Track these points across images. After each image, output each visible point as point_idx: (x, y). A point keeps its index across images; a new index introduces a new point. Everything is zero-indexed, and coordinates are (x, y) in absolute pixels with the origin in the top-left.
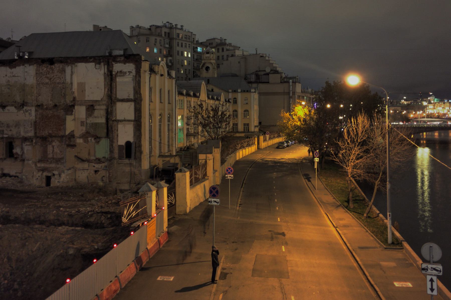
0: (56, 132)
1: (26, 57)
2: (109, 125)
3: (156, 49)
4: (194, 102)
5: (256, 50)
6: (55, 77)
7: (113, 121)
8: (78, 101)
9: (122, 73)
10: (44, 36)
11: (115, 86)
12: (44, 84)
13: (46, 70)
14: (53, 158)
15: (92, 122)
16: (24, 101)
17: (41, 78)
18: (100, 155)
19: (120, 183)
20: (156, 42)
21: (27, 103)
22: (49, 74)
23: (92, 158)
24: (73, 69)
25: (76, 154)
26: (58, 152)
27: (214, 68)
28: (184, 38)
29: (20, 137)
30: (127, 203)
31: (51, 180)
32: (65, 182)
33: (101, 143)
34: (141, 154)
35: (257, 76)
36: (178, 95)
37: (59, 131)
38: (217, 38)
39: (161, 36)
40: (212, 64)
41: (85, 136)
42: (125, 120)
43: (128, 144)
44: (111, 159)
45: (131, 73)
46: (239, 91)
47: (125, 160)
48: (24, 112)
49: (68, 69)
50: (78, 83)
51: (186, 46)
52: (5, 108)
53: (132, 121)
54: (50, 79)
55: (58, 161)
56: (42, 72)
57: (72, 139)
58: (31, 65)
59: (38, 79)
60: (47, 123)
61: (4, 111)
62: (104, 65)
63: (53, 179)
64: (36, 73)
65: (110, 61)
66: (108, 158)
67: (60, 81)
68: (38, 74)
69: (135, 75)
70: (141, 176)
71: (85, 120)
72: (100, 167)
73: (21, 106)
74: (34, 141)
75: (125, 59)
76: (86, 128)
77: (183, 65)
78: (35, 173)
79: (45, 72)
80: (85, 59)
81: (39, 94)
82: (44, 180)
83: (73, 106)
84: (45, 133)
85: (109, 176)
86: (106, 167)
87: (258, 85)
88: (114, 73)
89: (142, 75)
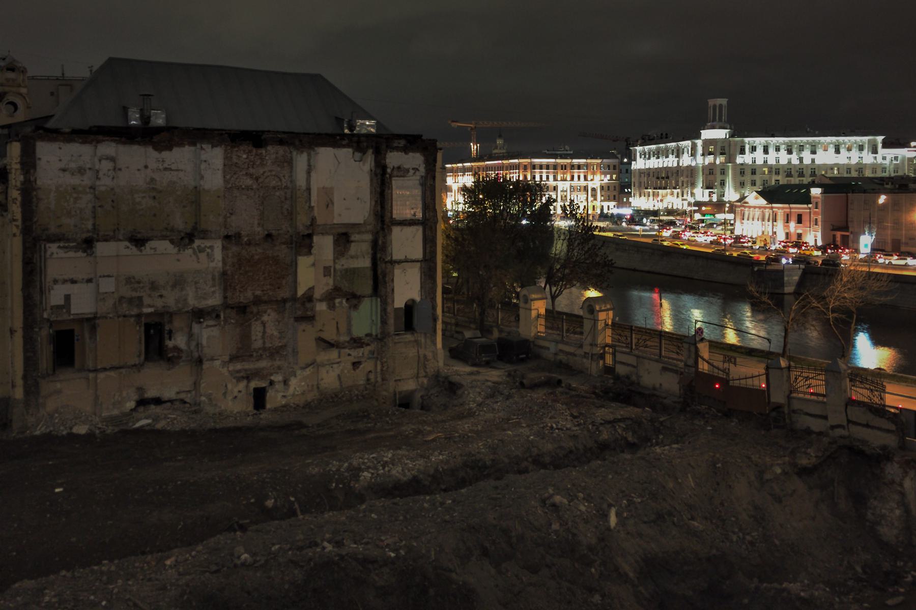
0: (271, 294)
2: (379, 271)
7: (386, 262)
9: (402, 171)
12: (243, 189)
13: (246, 159)
14: (264, 349)
15: (345, 267)
17: (235, 176)
19: (400, 380)
21: (207, 231)
22: (253, 167)
23: (344, 338)
24: (312, 161)
26: (276, 333)
29: (186, 309)
32: (297, 395)
37: (277, 290)
41: (329, 298)
42: (406, 261)
43: (410, 308)
44: (382, 338)
45: (417, 172)
47: (405, 336)
48: (195, 253)
49: (301, 161)
53: (418, 261)
54: (257, 179)
55: (275, 352)
56: (236, 163)
58: (216, 146)
59: (228, 177)
60: (250, 274)
61: (141, 251)
63: (270, 394)
66: (377, 336)
67: (279, 184)
68: (229, 167)
69: (423, 174)
70: (438, 362)
71: (331, 264)
72: (361, 354)
78: (230, 386)
79: (245, 163)
81: (231, 211)
83: (310, 236)
85: (382, 370)
86: (372, 352)
88: (389, 170)
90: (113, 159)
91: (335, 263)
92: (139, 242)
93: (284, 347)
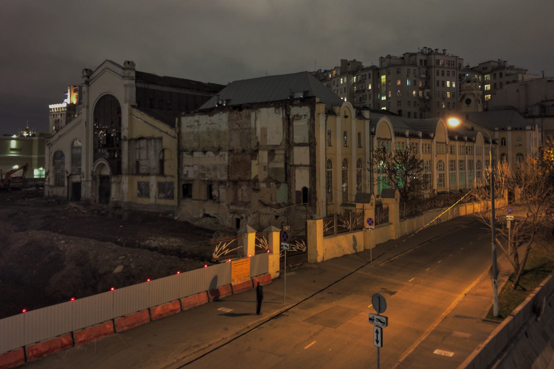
1: (224, 105)
3: (409, 81)
4: (426, 145)
5: (543, 73)
6: (243, 123)
7: (291, 166)
8: (261, 146)
9: (298, 117)
10: (243, 81)
11: (292, 130)
14: (242, 202)
15: (272, 167)
16: (219, 147)
18: (280, 201)
20: (408, 72)
25: (260, 199)
26: (246, 195)
27: (476, 101)
28: (446, 64)
30: (219, 241)
31: (240, 222)
33: (281, 188)
34: (316, 201)
35: (543, 108)
36: (395, 136)
38: (493, 60)
39: (416, 65)
40: (475, 96)
41: (268, 181)
43: (305, 189)
44: (290, 204)
45: (306, 117)
46: (509, 128)
50: (261, 129)
51: (448, 75)
52: (206, 153)
53: (307, 166)
54: (239, 125)
57: (257, 184)
59: (230, 125)
61: (205, 155)
62: (283, 109)
64: (229, 120)
65: (288, 105)
68: (230, 120)
69: (309, 118)
71: (267, 165)
72: (280, 212)
73: (217, 151)
74: (227, 185)
75: (301, 102)
76: (268, 173)
77: (444, 98)
78: (228, 215)
80: (266, 104)
82: (235, 223)
83: (257, 151)
84: (236, 177)
87: (304, 141)
88: (291, 117)
89: (316, 118)
90: (198, 121)
91: (268, 164)
92: (205, 152)
93: (249, 202)
